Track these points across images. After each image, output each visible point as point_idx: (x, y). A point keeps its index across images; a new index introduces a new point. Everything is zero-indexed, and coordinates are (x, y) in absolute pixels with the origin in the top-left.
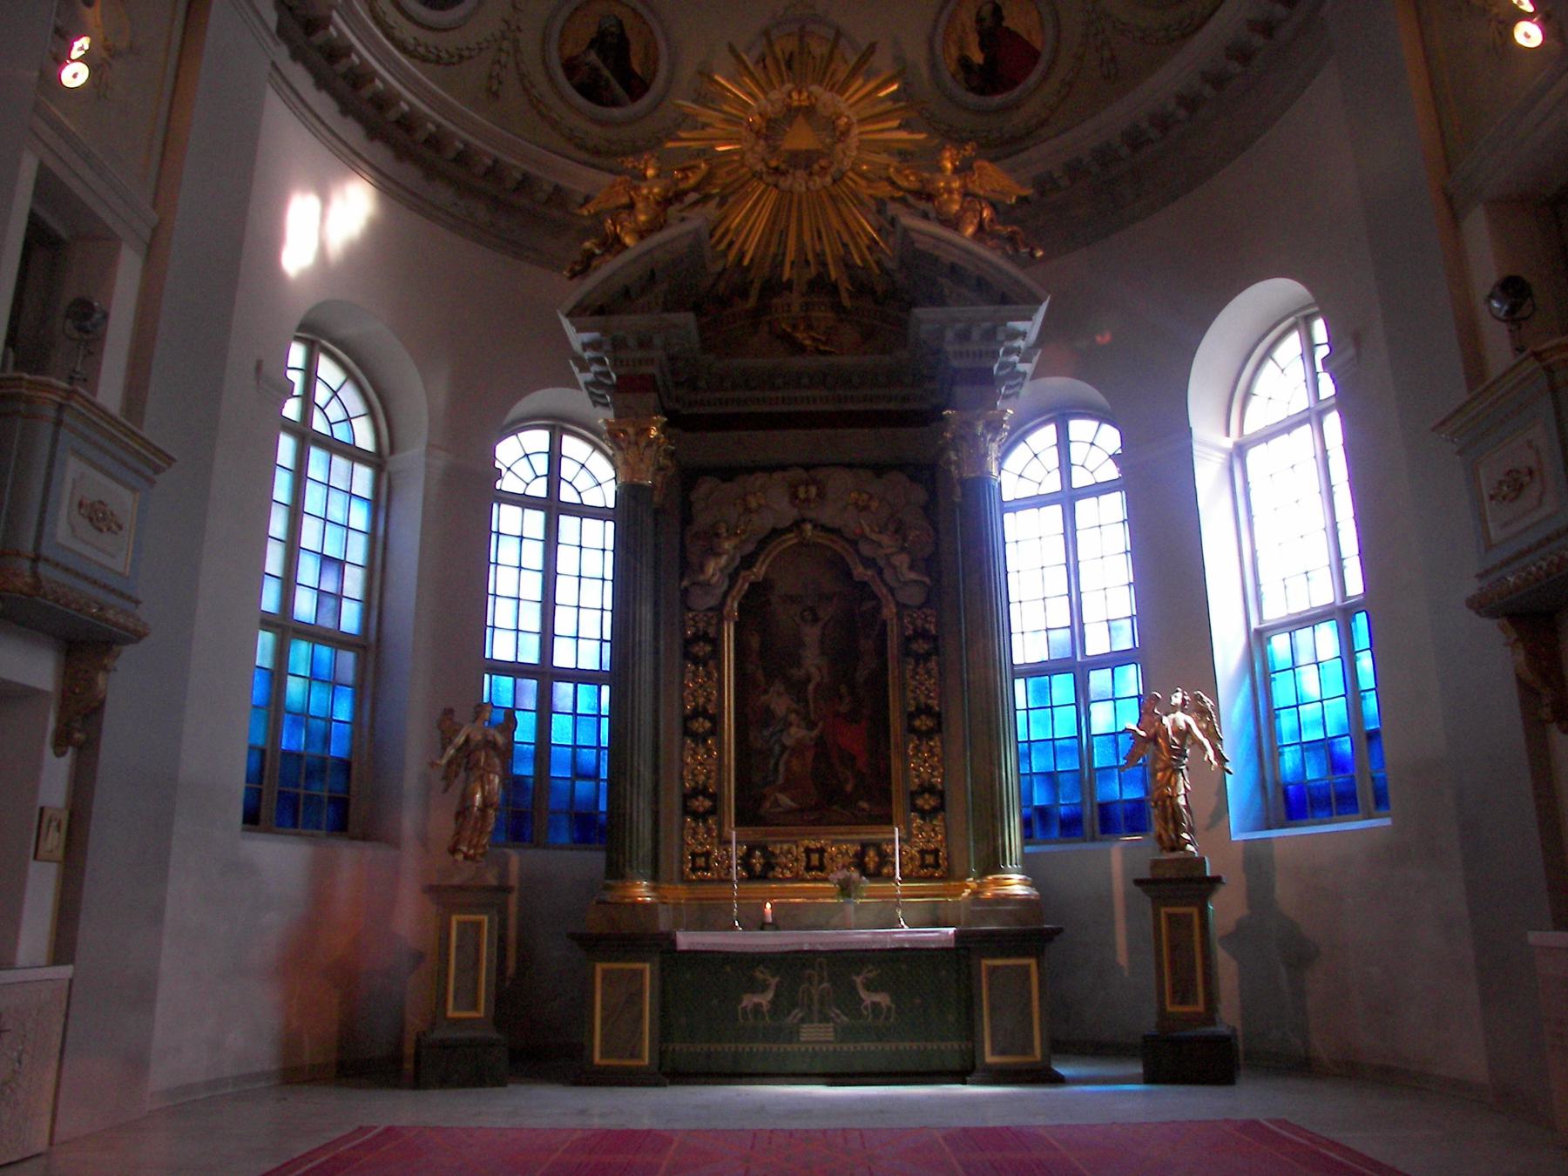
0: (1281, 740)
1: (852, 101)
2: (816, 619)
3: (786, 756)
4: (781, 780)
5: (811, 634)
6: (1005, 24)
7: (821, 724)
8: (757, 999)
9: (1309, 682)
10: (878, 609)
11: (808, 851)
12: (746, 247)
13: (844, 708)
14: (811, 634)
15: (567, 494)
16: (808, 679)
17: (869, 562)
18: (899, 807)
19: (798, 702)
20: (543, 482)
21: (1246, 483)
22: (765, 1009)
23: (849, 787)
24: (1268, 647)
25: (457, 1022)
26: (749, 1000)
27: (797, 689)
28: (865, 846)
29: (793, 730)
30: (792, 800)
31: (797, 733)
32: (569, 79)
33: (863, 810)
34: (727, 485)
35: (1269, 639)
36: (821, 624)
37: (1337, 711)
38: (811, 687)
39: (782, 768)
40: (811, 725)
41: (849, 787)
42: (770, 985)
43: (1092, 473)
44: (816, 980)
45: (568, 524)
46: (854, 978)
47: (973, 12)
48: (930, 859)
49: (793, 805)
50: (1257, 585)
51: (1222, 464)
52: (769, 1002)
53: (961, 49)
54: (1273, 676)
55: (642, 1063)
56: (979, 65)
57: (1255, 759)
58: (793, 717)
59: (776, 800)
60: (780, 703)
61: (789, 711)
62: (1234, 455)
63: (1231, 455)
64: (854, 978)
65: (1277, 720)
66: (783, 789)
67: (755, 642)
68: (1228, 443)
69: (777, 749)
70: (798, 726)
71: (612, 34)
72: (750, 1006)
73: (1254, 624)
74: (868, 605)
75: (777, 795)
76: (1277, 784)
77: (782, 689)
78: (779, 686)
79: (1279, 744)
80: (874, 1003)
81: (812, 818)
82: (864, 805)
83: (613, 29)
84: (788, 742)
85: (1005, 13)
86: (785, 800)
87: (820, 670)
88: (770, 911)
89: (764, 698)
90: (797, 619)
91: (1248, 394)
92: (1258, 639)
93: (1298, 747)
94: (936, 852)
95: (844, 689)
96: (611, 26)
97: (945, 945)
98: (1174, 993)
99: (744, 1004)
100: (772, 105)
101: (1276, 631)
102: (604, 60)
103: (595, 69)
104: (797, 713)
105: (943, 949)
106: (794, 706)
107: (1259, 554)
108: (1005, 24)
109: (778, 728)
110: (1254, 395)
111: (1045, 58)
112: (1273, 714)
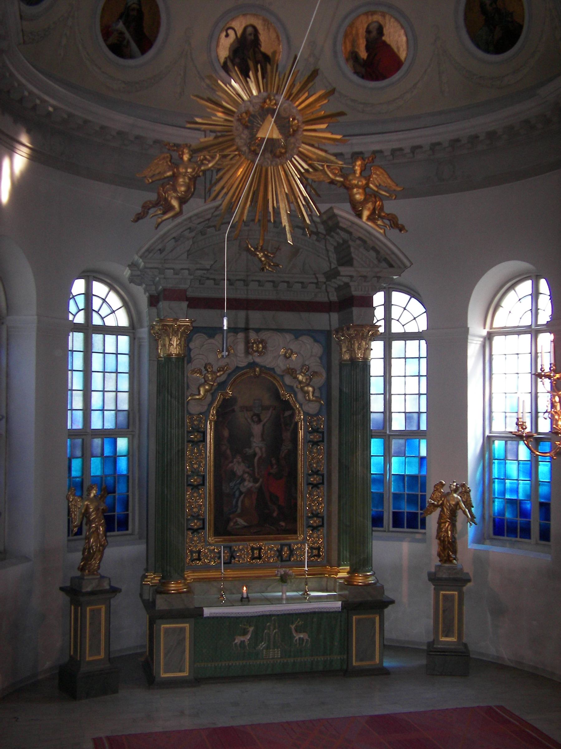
0: (494, 494)
1: (299, 108)
2: (260, 421)
3: (242, 496)
4: (239, 511)
5: (257, 429)
6: (384, 38)
7: (261, 480)
8: (242, 638)
9: (512, 469)
10: (293, 415)
11: (253, 549)
12: (225, 185)
13: (274, 470)
14: (257, 429)
15: (97, 320)
16: (255, 455)
17: (291, 389)
18: (301, 523)
19: (249, 467)
20: (82, 313)
21: (491, 355)
22: (247, 643)
23: (275, 514)
24: (493, 446)
25: (90, 662)
26: (238, 640)
27: (248, 459)
28: (282, 545)
29: (246, 483)
30: (245, 521)
31: (248, 484)
32: (105, 40)
33: (282, 526)
34: (212, 341)
35: (494, 441)
36: (262, 423)
37: (524, 486)
38: (256, 459)
39: (240, 504)
40: (256, 481)
41: (275, 514)
42: (249, 631)
43: (403, 326)
44: (272, 628)
45: (97, 339)
46: (291, 626)
47: (365, 26)
48: (315, 552)
49: (245, 524)
50: (491, 412)
51: (480, 344)
52: (249, 640)
53: (353, 46)
54: (494, 461)
55: (90, 608)
56: (363, 59)
57: (481, 503)
58: (246, 476)
59: (236, 521)
60: (239, 468)
61: (244, 472)
62: (487, 339)
63: (485, 338)
64: (291, 626)
65: (493, 484)
66: (240, 516)
67: (226, 433)
68: (484, 333)
69: (237, 493)
70: (249, 481)
71: (133, 9)
72: (239, 642)
73: (487, 433)
74: (287, 413)
75: (237, 519)
76: (490, 517)
77: (240, 460)
78: (239, 458)
79: (493, 496)
80: (300, 638)
81: (255, 531)
82: (283, 524)
83: (134, 6)
84: (243, 490)
85: (385, 31)
86: (241, 521)
87: (261, 449)
88: (246, 591)
89: (230, 465)
90: (249, 420)
91: (498, 306)
92: (488, 441)
93: (502, 500)
94: (318, 549)
95: (274, 461)
96: (134, 3)
97: (337, 610)
98: (443, 632)
99: (236, 641)
100: (253, 106)
101: (497, 438)
102: (128, 28)
103: (121, 33)
104: (248, 473)
105: (336, 612)
106: (247, 470)
107: (493, 395)
108: (384, 38)
109: (238, 482)
110: (502, 307)
111: (404, 68)
112: (491, 481)
